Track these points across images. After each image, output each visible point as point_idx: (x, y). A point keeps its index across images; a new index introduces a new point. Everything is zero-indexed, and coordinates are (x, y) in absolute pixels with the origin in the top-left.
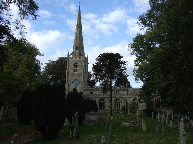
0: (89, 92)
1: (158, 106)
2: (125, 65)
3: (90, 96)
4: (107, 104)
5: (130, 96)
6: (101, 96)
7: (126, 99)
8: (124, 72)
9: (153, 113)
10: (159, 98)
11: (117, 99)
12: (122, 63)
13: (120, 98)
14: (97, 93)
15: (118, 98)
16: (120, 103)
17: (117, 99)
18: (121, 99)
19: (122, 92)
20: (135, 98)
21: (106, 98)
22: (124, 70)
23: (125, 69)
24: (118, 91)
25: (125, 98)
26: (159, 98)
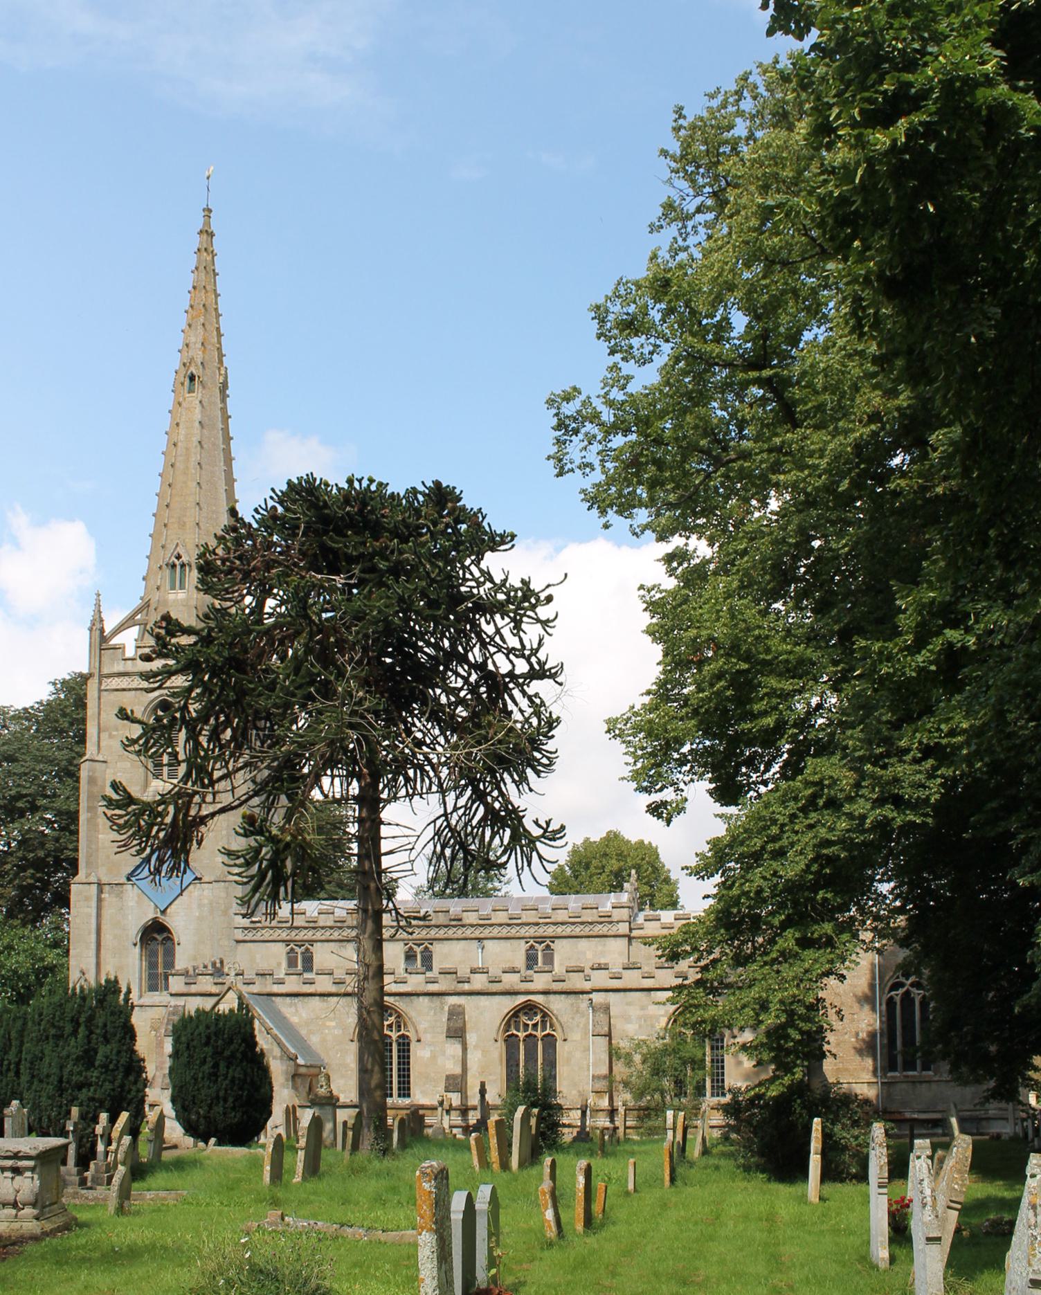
0: (280, 950)
1: (909, 1065)
2: (532, 632)
3: (276, 989)
4: (434, 1057)
5: (648, 983)
6: (281, 982)
7: (606, 1009)
8: (524, 703)
9: (961, 1121)
10: (917, 994)
11: (529, 1008)
12: (501, 608)
13: (552, 997)
14: (587, 951)
15: (539, 999)
16: (550, 1041)
17: (529, 1008)
18: (557, 1005)
19: (583, 943)
20: (521, 999)
21: (424, 1000)
22: (535, 687)
23: (539, 673)
24: (540, 939)
25: (597, 998)
26: (917, 994)
